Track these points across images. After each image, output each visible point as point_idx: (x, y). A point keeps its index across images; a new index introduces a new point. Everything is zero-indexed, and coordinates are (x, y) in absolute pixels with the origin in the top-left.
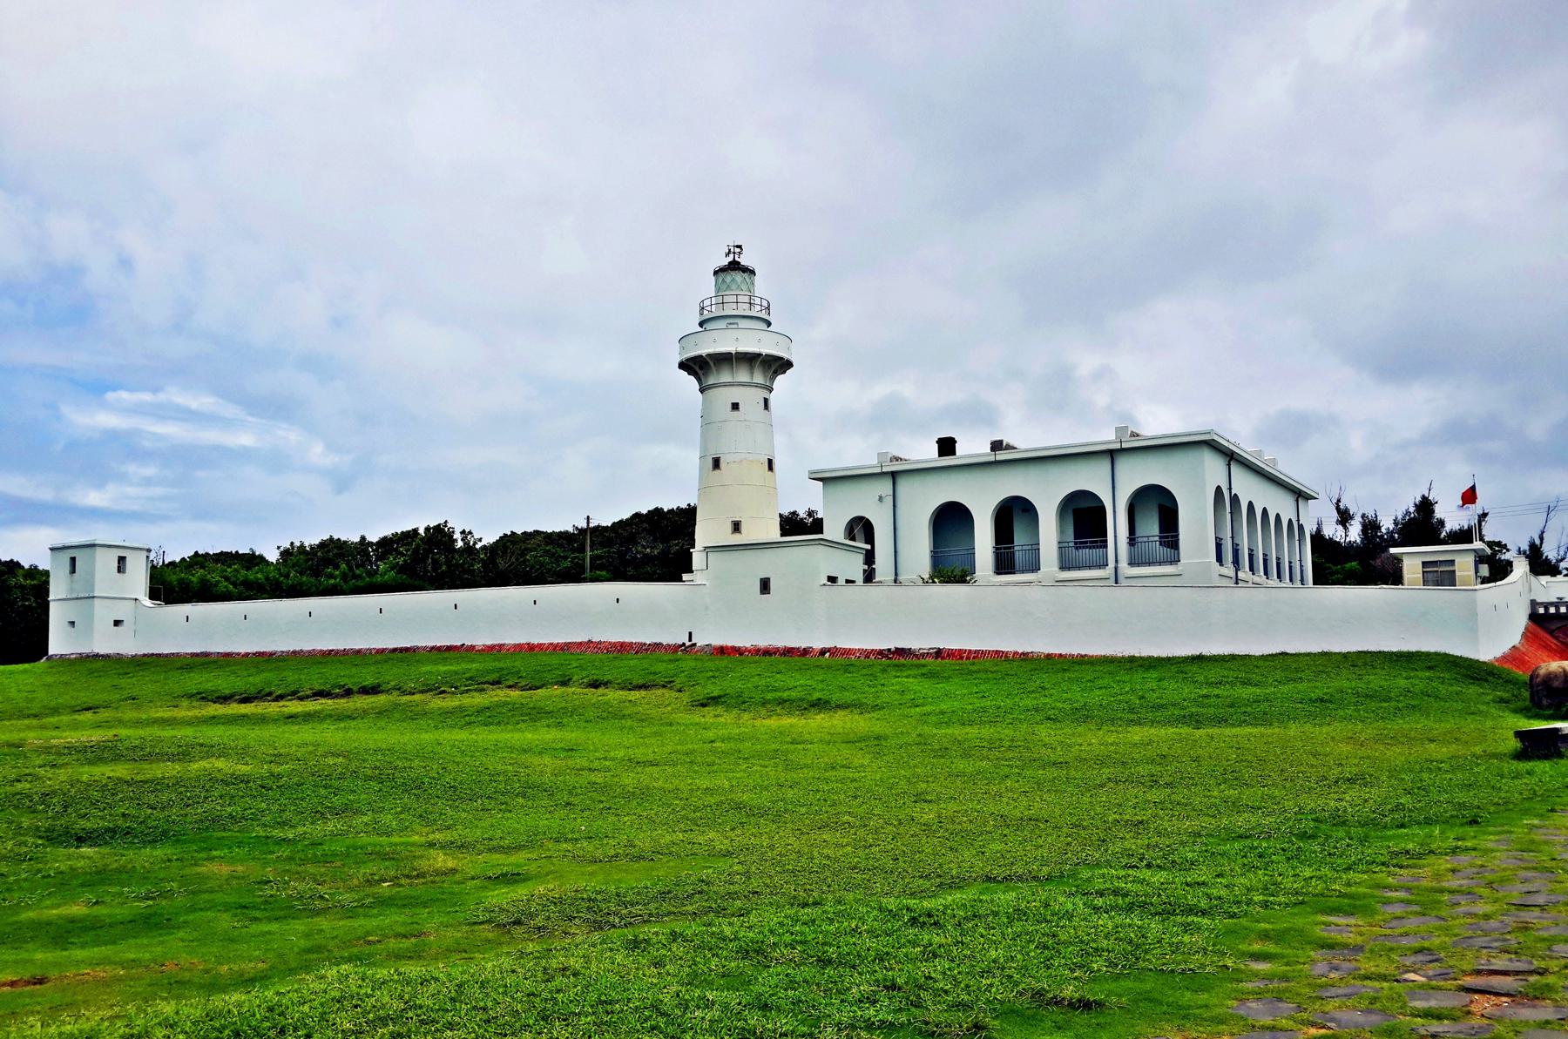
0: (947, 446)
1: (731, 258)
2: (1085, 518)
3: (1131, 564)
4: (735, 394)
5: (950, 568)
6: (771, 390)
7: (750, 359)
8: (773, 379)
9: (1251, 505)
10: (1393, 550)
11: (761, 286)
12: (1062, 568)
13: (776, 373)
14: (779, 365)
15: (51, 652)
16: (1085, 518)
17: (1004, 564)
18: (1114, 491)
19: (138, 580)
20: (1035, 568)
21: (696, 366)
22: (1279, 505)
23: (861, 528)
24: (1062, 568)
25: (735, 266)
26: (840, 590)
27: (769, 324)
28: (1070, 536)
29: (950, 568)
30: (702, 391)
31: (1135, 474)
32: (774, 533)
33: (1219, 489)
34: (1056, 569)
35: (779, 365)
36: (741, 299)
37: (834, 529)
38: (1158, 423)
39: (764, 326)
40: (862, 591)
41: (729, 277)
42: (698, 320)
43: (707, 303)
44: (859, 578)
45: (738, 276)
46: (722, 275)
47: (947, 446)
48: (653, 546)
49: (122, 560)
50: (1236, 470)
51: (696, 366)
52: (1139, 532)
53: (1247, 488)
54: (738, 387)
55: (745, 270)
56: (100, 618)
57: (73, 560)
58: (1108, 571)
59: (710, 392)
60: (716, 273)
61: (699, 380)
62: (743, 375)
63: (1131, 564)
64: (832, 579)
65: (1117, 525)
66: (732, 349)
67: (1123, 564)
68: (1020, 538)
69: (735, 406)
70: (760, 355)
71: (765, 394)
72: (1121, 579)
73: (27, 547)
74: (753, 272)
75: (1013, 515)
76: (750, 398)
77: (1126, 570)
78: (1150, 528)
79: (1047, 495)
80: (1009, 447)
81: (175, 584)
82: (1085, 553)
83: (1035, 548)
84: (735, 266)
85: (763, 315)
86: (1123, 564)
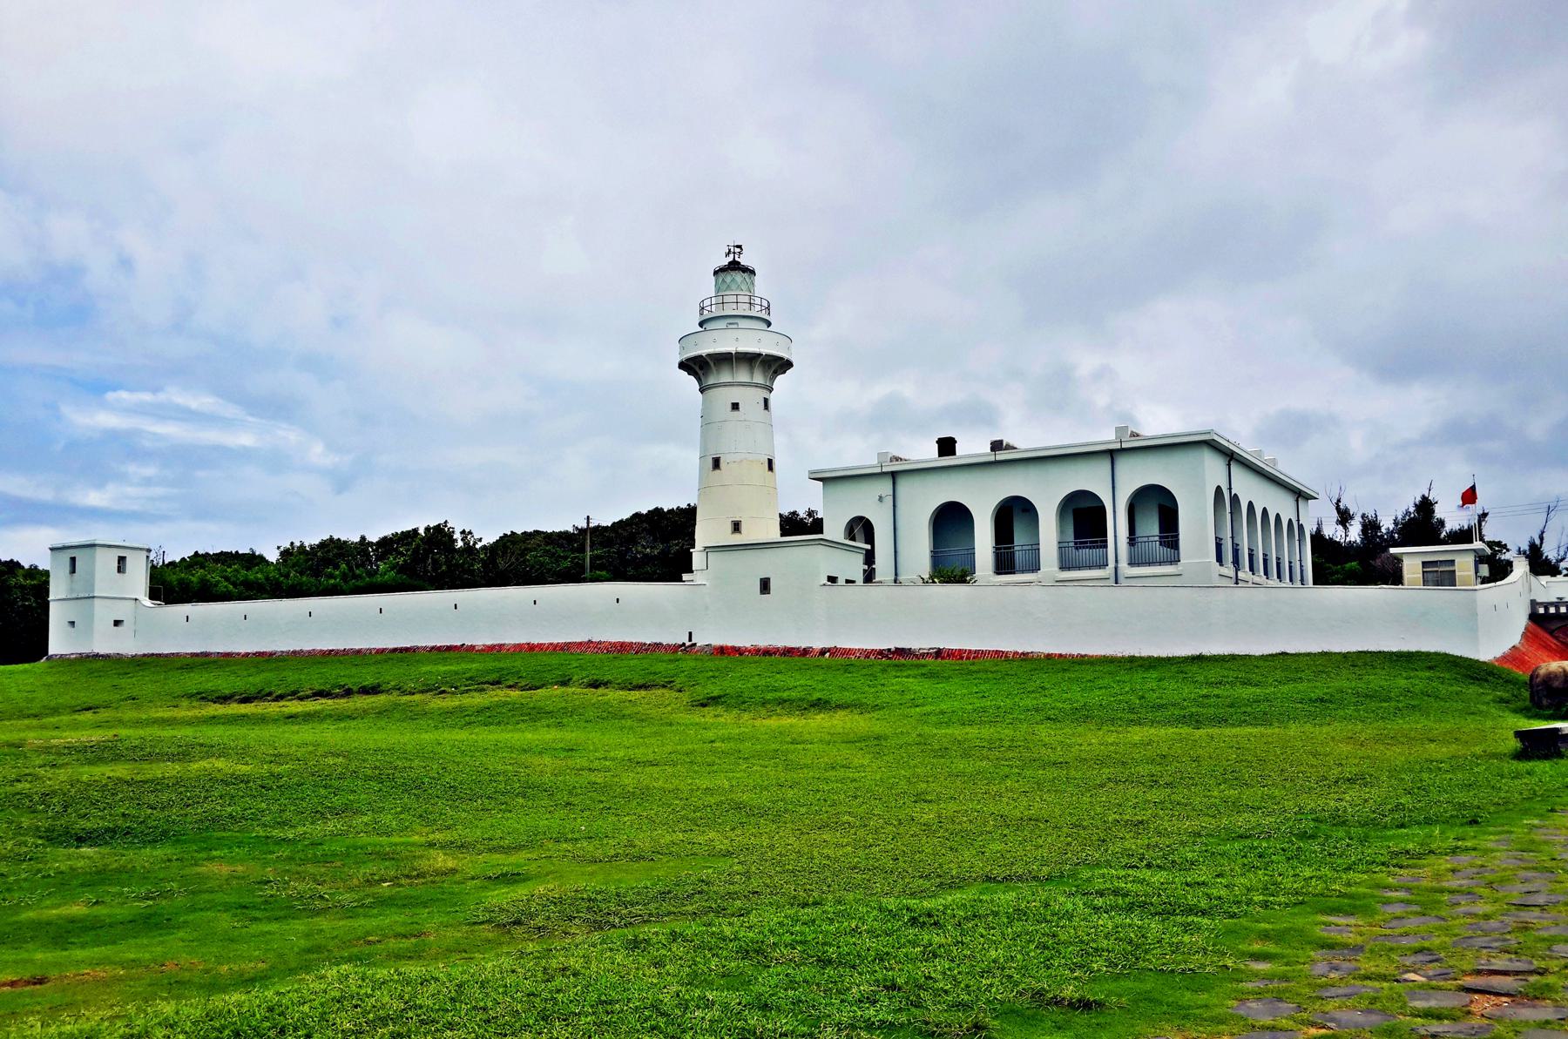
0: (947, 446)
1: (731, 258)
2: (1085, 518)
3: (1131, 564)
4: (735, 394)
5: (950, 568)
6: (771, 390)
7: (750, 359)
8: (773, 380)
9: (1251, 505)
10: (1393, 550)
11: (761, 286)
12: (1062, 568)
13: (776, 373)
14: (779, 365)
15: (51, 652)
16: (1085, 518)
17: (1004, 564)
18: (1114, 491)
19: (138, 580)
20: (1035, 568)
21: (696, 366)
22: (1279, 505)
23: (861, 528)
24: (1062, 568)
25: (734, 266)
26: (840, 590)
27: (769, 324)
28: (1070, 536)
29: (950, 568)
30: (702, 391)
31: (1135, 474)
32: (774, 533)
33: (1219, 489)
34: (1056, 569)
35: (779, 365)
36: (740, 299)
37: (834, 529)
38: (1158, 423)
39: (764, 326)
40: (861, 591)
41: (729, 277)
42: (698, 319)
43: (707, 303)
44: (859, 578)
45: (738, 276)
46: (722, 275)
47: (947, 446)
48: (653, 546)
49: (122, 560)
50: (1236, 470)
51: (696, 366)
52: (1139, 532)
53: (1247, 488)
54: (738, 387)
55: (745, 270)
56: (100, 618)
57: (73, 560)
58: (1108, 571)
59: (710, 392)
60: (716, 273)
61: (699, 380)
62: (743, 375)
63: (1131, 564)
64: (832, 579)
65: (1117, 525)
66: (732, 349)
67: (1123, 564)
68: (1020, 538)
69: (735, 406)
70: (760, 355)
71: (765, 394)
72: (1121, 579)
73: (27, 547)
74: (753, 272)
75: (1013, 515)
76: (750, 398)
77: (1126, 570)
78: (1150, 528)
79: (1047, 495)
80: (1009, 447)
81: (175, 584)
82: (1086, 553)
83: (1035, 549)
84: (734, 266)
85: (763, 315)
86: (1123, 564)
